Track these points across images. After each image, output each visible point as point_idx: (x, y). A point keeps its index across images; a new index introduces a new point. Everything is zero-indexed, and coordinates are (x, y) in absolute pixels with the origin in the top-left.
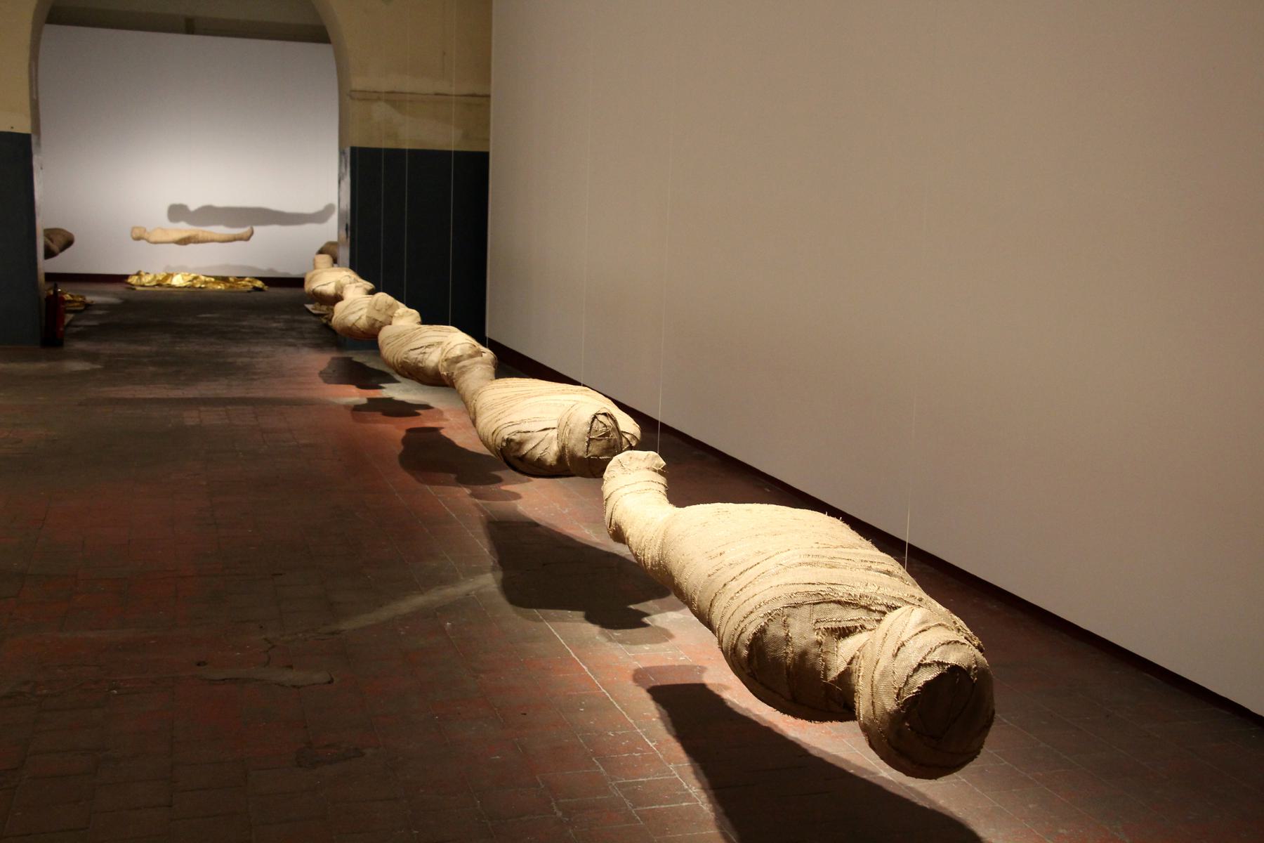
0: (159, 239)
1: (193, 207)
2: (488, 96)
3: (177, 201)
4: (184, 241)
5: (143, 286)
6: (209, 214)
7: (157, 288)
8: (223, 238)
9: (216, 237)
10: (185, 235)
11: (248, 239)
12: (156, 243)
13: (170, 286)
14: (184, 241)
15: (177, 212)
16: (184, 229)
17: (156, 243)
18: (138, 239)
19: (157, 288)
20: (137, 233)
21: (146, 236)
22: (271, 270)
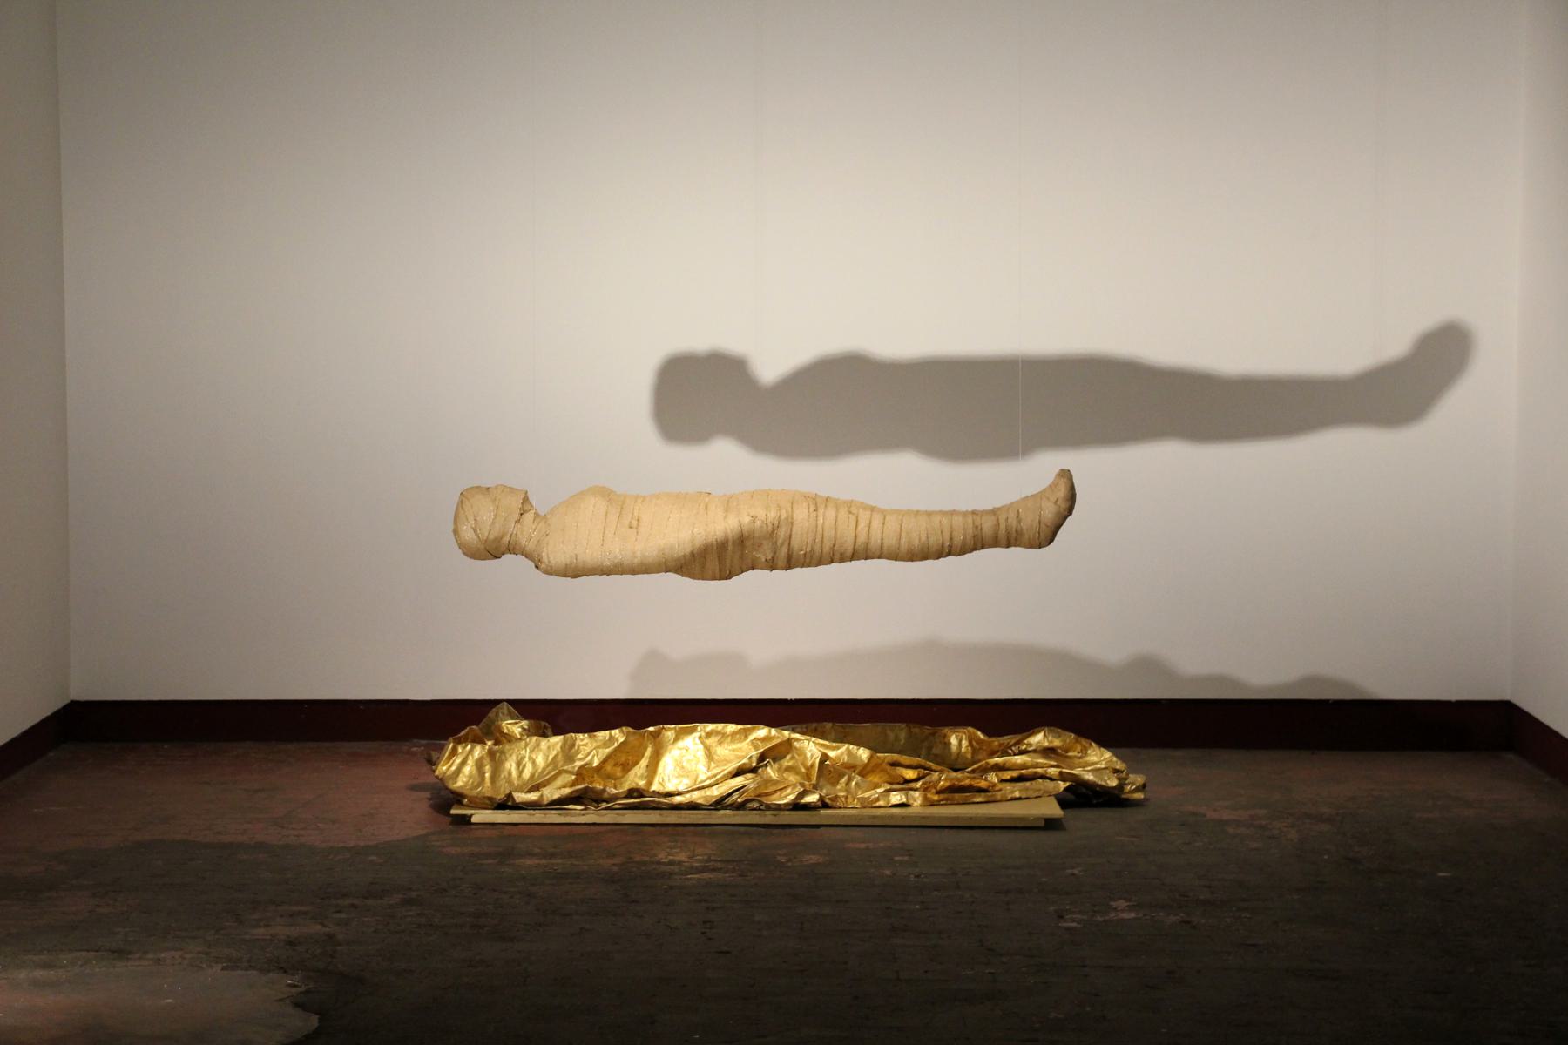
0: (590, 553)
1: (772, 363)
2: (772, 569)
3: (700, 341)
4: (719, 560)
5: (507, 804)
6: (851, 400)
7: (578, 814)
8: (917, 532)
9: (881, 532)
10: (720, 525)
11: (1046, 536)
12: (575, 572)
13: (638, 798)
14: (719, 560)
15: (700, 394)
16: (735, 481)
17: (575, 572)
18: (492, 551)
19: (578, 814)
20: (486, 519)
21: (527, 532)
22: (1147, 665)
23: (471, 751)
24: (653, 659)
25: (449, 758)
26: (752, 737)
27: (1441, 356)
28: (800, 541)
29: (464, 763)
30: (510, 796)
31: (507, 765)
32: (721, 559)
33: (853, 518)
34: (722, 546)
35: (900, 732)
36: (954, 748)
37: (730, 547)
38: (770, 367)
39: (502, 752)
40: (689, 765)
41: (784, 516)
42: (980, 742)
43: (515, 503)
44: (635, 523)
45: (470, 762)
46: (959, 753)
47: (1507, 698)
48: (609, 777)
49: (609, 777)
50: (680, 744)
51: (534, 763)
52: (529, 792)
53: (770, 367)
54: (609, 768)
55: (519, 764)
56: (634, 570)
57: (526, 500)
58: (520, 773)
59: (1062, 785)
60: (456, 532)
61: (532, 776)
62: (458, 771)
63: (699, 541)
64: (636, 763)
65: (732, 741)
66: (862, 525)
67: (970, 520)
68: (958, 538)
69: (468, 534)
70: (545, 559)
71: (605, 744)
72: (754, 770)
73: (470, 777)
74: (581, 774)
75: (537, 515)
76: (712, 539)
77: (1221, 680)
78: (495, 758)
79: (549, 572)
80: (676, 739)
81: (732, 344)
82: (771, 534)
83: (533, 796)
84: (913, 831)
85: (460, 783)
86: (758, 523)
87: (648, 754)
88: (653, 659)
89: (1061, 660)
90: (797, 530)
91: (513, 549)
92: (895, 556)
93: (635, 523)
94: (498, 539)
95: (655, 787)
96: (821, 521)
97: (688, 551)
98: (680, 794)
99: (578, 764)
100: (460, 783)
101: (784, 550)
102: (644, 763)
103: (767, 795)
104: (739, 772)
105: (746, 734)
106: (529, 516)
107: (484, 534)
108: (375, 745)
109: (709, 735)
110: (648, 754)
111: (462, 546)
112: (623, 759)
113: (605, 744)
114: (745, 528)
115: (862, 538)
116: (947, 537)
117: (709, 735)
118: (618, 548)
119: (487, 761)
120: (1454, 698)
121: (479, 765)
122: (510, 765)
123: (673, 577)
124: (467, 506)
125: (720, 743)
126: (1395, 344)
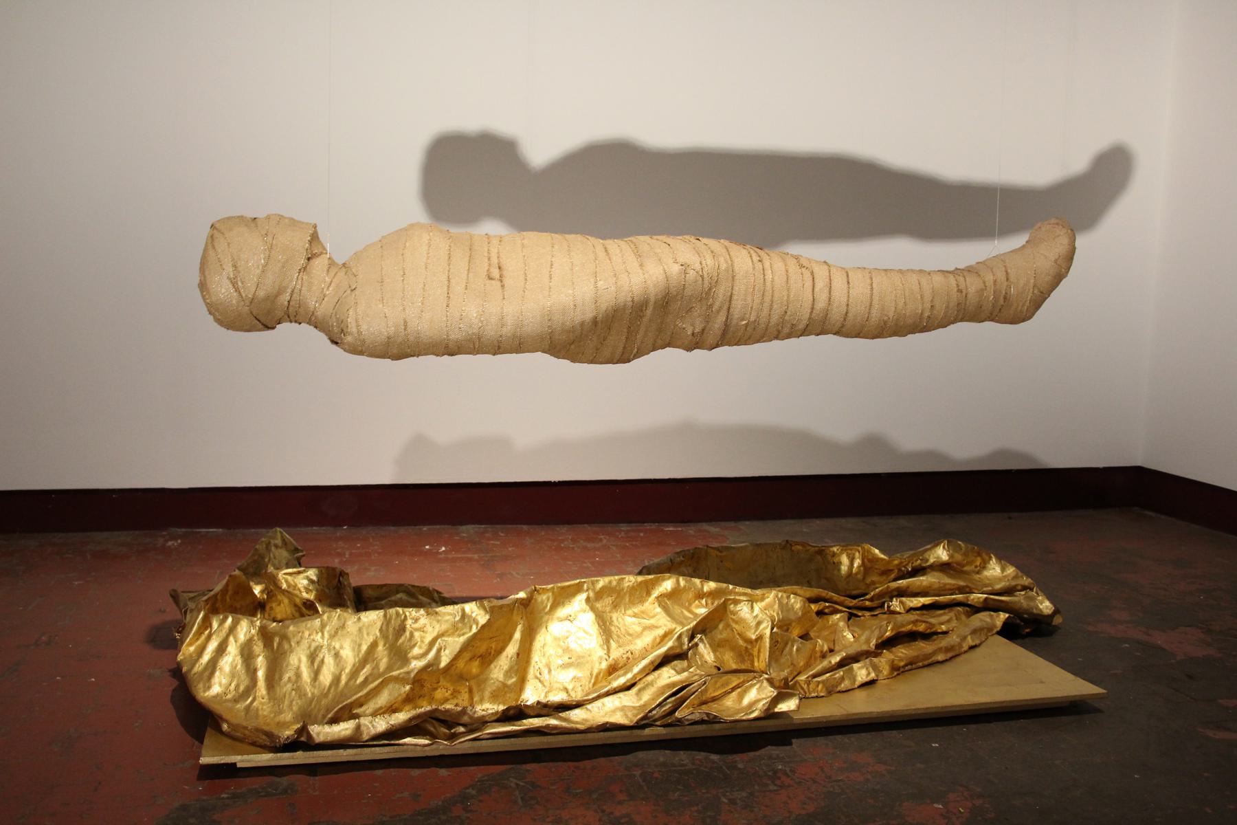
0: (428, 318)
3: (470, 122)
12: (398, 349)
15: (470, 175)
18: (263, 316)
20: (252, 269)
21: (318, 288)
22: (873, 443)
23: (232, 630)
24: (419, 444)
25: (199, 633)
26: (656, 593)
27: (1111, 172)
28: (744, 304)
29: (221, 650)
30: (303, 730)
31: (293, 660)
32: (631, 333)
33: (807, 274)
34: (638, 309)
35: (738, 537)
36: (844, 569)
37: (649, 312)
38: (541, 150)
39: (285, 637)
40: (590, 650)
41: (723, 266)
42: (875, 560)
43: (300, 242)
44: (495, 273)
45: (233, 649)
46: (850, 574)
47: (1139, 464)
48: (462, 677)
49: (462, 677)
50: (562, 612)
51: (337, 655)
52: (334, 721)
53: (541, 150)
54: (461, 664)
55: (312, 657)
56: (498, 347)
57: (315, 237)
58: (316, 674)
59: (1003, 616)
60: (203, 286)
61: (336, 679)
62: (213, 665)
63: (606, 303)
64: (502, 649)
65: (632, 603)
66: (820, 284)
67: (914, 278)
68: (940, 308)
69: (223, 290)
70: (352, 328)
71: (455, 629)
72: (682, 656)
73: (233, 675)
74: (422, 682)
75: (332, 263)
76: (624, 297)
77: (931, 455)
78: (274, 646)
79: (358, 349)
80: (555, 606)
81: (502, 126)
82: (705, 296)
83: (344, 729)
84: (935, 741)
85: (216, 689)
86: (692, 275)
87: (517, 635)
88: (419, 444)
89: (803, 440)
90: (740, 288)
91: (295, 314)
92: (842, 331)
93: (495, 273)
94: (272, 298)
95: (531, 695)
96: (769, 276)
97: (589, 316)
98: (578, 705)
99: (416, 665)
100: (216, 689)
101: (721, 318)
102: (512, 649)
103: (714, 699)
104: (665, 661)
105: (647, 588)
106: (319, 264)
107: (249, 289)
108: (124, 536)
109: (599, 595)
110: (517, 635)
111: (212, 309)
112: (482, 648)
113: (455, 629)
114: (391, 333)
115: (821, 305)
116: (928, 305)
117: (599, 595)
118: (476, 311)
119: (258, 647)
120: (1101, 465)
121: (247, 655)
122: (298, 659)
123: (541, 360)
124: (221, 245)
125: (615, 606)
126: (1078, 163)
